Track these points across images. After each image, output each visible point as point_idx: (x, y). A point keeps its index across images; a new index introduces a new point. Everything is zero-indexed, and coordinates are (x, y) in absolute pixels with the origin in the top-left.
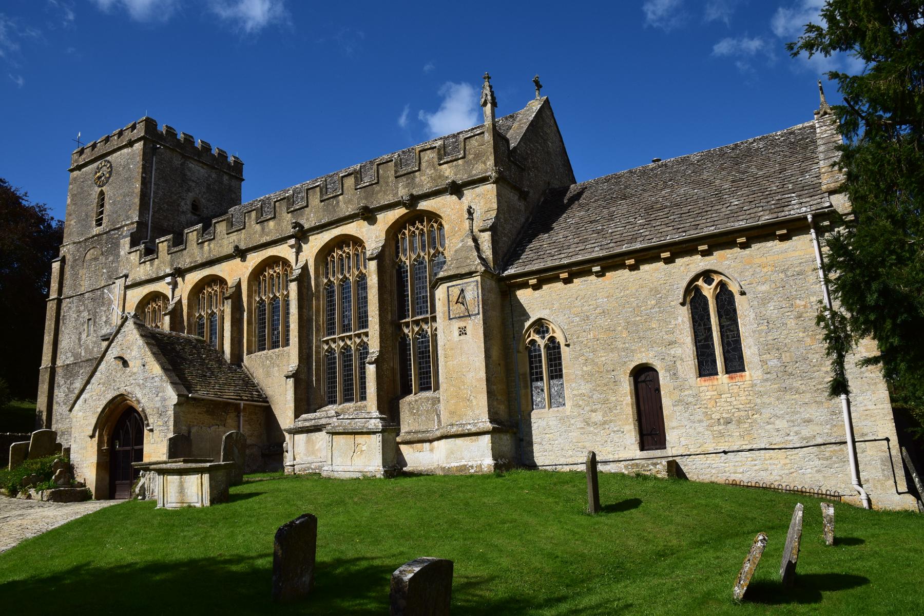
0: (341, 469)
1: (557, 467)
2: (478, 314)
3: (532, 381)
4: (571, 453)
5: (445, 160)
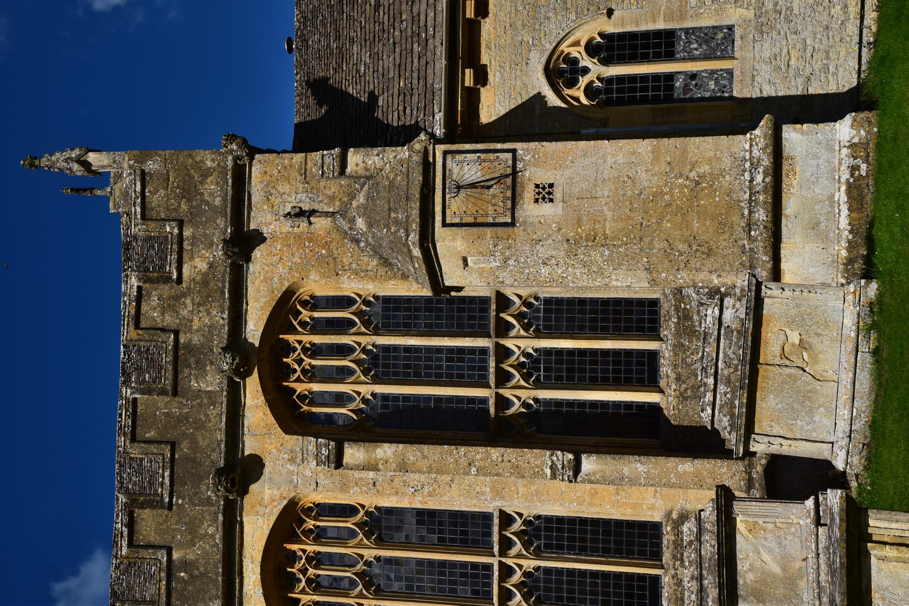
0: (846, 413)
1: (865, 39)
2: (514, 151)
3: (669, 98)
4: (838, 8)
5: (174, 266)
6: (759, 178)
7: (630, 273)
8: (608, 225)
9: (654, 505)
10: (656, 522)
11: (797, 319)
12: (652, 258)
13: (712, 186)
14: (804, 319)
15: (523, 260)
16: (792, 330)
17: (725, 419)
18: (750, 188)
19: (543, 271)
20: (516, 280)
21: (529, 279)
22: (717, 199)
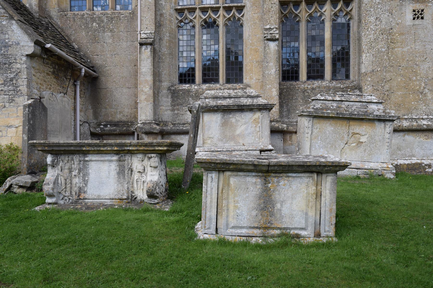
6: (425, 122)
7: (371, 63)
8: (400, 49)
9: (253, 79)
10: (243, 81)
11: (373, 140)
12: (380, 73)
13: (420, 100)
14: (373, 143)
15: (379, 7)
16: (367, 138)
17: (319, 106)
18: (418, 119)
19: (372, 18)
20: (366, 4)
21: (367, 11)
22: (413, 103)
